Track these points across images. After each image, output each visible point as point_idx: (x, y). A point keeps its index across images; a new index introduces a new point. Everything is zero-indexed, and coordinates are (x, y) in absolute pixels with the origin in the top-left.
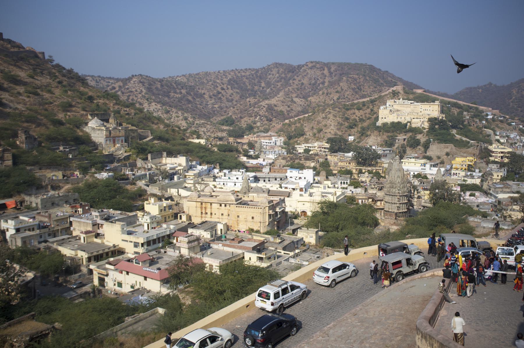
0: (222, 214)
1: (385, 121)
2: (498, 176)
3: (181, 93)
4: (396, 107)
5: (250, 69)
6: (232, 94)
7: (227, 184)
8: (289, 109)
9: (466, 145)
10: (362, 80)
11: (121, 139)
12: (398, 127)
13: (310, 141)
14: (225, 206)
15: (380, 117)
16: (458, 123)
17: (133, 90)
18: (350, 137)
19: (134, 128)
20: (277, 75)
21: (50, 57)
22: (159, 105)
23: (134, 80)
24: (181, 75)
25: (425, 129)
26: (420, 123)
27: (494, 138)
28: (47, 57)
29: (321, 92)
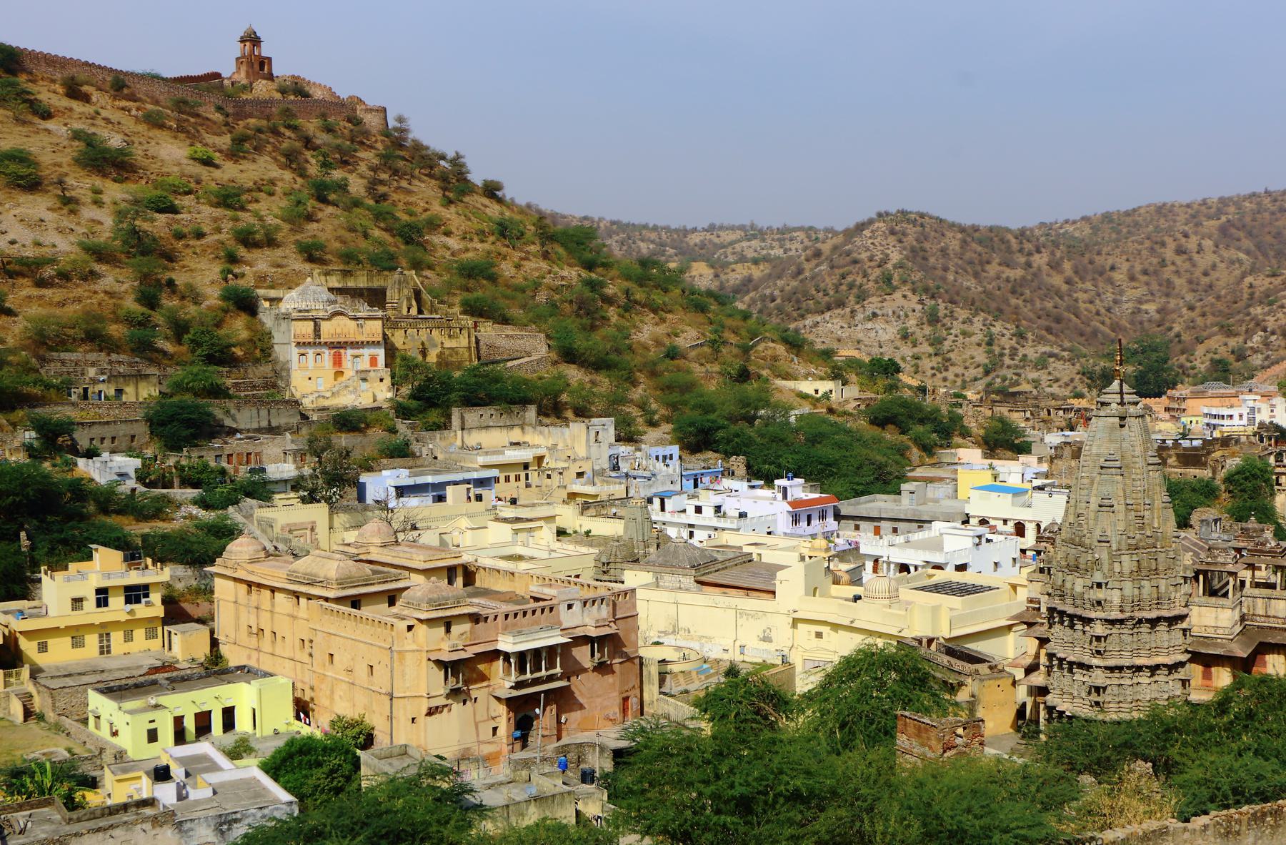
6: (1214, 267)
17: (864, 256)
21: (400, 119)
24: (1078, 218)
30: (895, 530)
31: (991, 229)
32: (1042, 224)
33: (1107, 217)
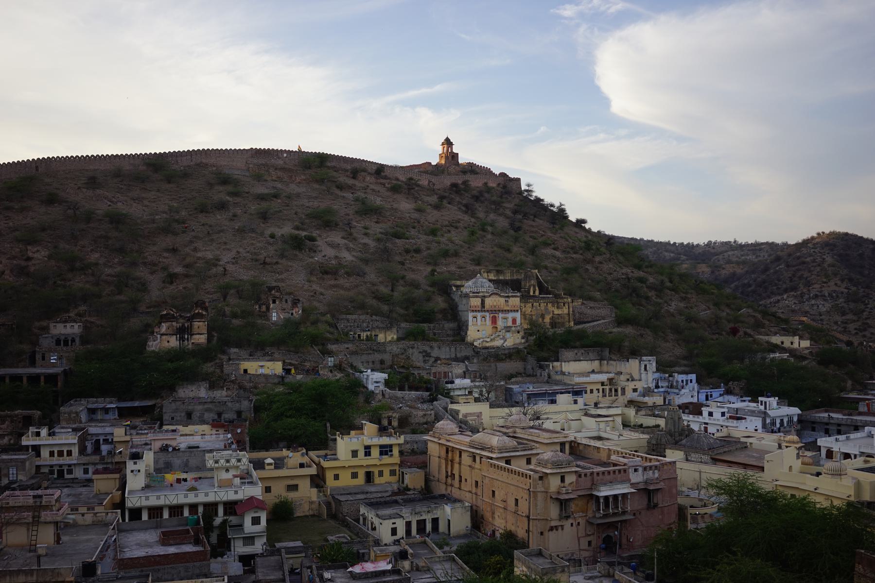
11: (510, 316)
21: (529, 185)
28: (524, 187)
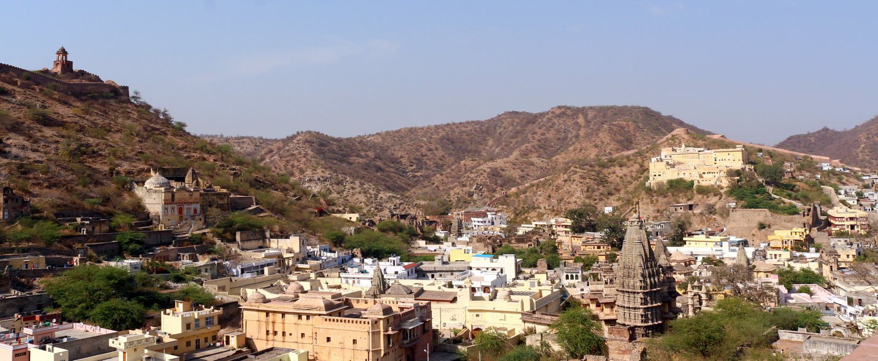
0: (303, 335)
1: (658, 179)
2: (848, 256)
3: (367, 156)
4: (676, 158)
5: (473, 122)
7: (359, 282)
8: (522, 174)
9: (792, 211)
10: (632, 128)
11: (193, 206)
12: (679, 187)
13: (545, 216)
14: (308, 318)
15: (652, 173)
16: (775, 178)
17: (296, 152)
18: (606, 208)
19: (225, 191)
20: (511, 128)
21: (136, 93)
22: (327, 172)
23: (299, 138)
25: (722, 188)
26: (715, 180)
27: (835, 199)
28: (131, 94)
29: (571, 148)
30: (441, 275)
31: (347, 139)
32: (359, 137)
33: (387, 133)
